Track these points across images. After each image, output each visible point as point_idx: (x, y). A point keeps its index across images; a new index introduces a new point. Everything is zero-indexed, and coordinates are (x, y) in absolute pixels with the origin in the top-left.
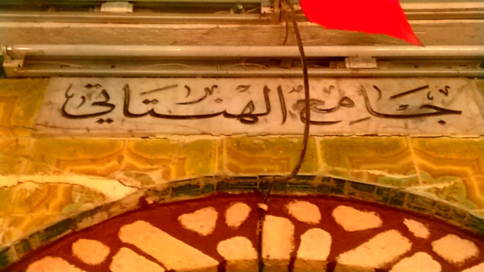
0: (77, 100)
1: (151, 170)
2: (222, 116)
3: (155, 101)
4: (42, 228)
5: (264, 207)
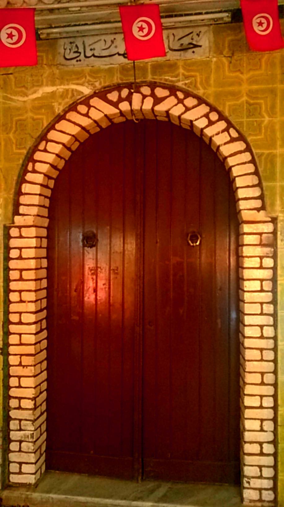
0: (68, 51)
1: (95, 82)
2: (117, 55)
3: (94, 49)
4: (67, 105)
5: (132, 91)
